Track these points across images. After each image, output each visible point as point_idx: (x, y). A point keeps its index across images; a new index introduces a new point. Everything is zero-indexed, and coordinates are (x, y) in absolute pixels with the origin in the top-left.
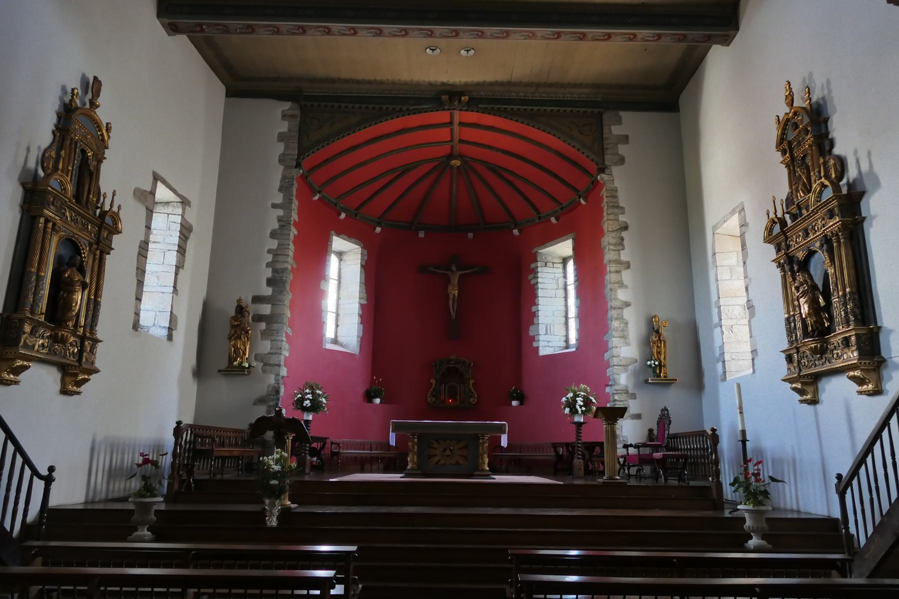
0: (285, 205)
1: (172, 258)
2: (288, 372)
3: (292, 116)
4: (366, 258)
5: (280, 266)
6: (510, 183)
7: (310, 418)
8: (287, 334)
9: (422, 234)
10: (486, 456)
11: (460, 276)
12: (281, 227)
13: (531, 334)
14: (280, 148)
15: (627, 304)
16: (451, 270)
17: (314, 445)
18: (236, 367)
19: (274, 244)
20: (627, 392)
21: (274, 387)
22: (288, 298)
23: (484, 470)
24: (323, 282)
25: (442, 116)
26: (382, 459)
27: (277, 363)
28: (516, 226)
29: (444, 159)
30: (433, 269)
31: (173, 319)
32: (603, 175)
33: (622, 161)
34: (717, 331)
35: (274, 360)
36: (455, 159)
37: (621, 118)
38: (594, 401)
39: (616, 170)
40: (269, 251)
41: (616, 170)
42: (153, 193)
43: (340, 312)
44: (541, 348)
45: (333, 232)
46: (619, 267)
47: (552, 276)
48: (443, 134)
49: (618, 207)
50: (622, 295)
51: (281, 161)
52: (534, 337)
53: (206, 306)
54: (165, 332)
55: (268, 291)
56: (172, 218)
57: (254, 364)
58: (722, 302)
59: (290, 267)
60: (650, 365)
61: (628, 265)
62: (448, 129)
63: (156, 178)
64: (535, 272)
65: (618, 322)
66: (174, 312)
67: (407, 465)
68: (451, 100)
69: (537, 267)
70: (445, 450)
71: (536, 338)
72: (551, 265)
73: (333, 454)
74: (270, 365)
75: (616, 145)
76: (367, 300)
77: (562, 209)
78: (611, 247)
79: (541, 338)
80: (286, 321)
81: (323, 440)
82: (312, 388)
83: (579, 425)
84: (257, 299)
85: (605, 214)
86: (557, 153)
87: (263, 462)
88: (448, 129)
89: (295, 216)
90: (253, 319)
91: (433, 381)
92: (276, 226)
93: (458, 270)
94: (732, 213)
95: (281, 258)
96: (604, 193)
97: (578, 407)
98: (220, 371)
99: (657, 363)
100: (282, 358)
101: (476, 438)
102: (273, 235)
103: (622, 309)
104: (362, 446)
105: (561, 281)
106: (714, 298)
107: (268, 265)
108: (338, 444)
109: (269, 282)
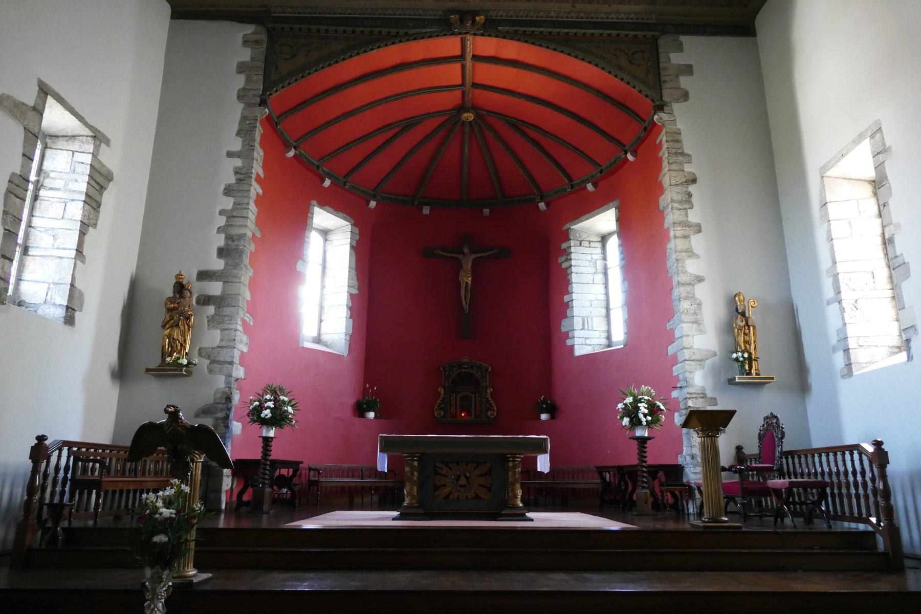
0: (246, 154)
1: (77, 210)
2: (246, 373)
3: (256, 42)
4: (357, 237)
5: (235, 231)
6: (537, 143)
7: (272, 433)
8: (244, 321)
9: (426, 211)
10: (518, 486)
11: (474, 259)
12: (239, 181)
13: (563, 329)
14: (240, 81)
15: (700, 279)
16: (463, 253)
17: (284, 472)
18: (169, 364)
19: (228, 203)
20: (704, 396)
21: (224, 393)
22: (246, 274)
23: (515, 507)
24: (300, 263)
25: (449, 45)
26: (377, 489)
27: (228, 359)
28: (542, 200)
29: (454, 112)
30: (440, 252)
31: (74, 292)
32: (661, 114)
33: (685, 96)
34: (833, 309)
35: (224, 355)
36: (468, 111)
37: (681, 44)
38: (662, 407)
39: (677, 107)
40: (222, 213)
41: (677, 107)
42: (39, 111)
43: (326, 304)
44: (576, 347)
45: (314, 202)
46: (687, 231)
47: (589, 257)
48: (451, 74)
49: (682, 154)
50: (692, 267)
51: (240, 98)
52: (567, 333)
53: (134, 285)
54: (61, 312)
55: (218, 264)
56: (79, 157)
57: (196, 360)
58: (840, 268)
59: (250, 234)
60: (737, 359)
61: (698, 229)
62: (457, 66)
63: (44, 91)
64: (567, 253)
65: (688, 302)
66: (77, 285)
67: (404, 501)
68: (462, 21)
69: (570, 247)
70: (458, 478)
71: (570, 336)
72: (587, 244)
73: (312, 483)
74: (219, 362)
75: (677, 76)
76: (359, 289)
77: (601, 172)
78: (676, 205)
79: (577, 334)
80: (243, 304)
81: (295, 465)
82: (274, 392)
83: (643, 441)
84: (204, 275)
85: (665, 163)
86: (599, 92)
87: (144, 505)
88: (457, 66)
89: (258, 169)
90: (198, 302)
91: (441, 390)
92: (232, 180)
93: (472, 251)
94: (860, 138)
95: (238, 222)
96: (663, 137)
97: (641, 416)
98: (147, 370)
99: (746, 355)
100: (237, 354)
101: (504, 459)
102: (228, 191)
103: (693, 285)
104: (351, 472)
105: (600, 264)
106: (825, 262)
107: (220, 230)
108: (318, 470)
109: (221, 252)
